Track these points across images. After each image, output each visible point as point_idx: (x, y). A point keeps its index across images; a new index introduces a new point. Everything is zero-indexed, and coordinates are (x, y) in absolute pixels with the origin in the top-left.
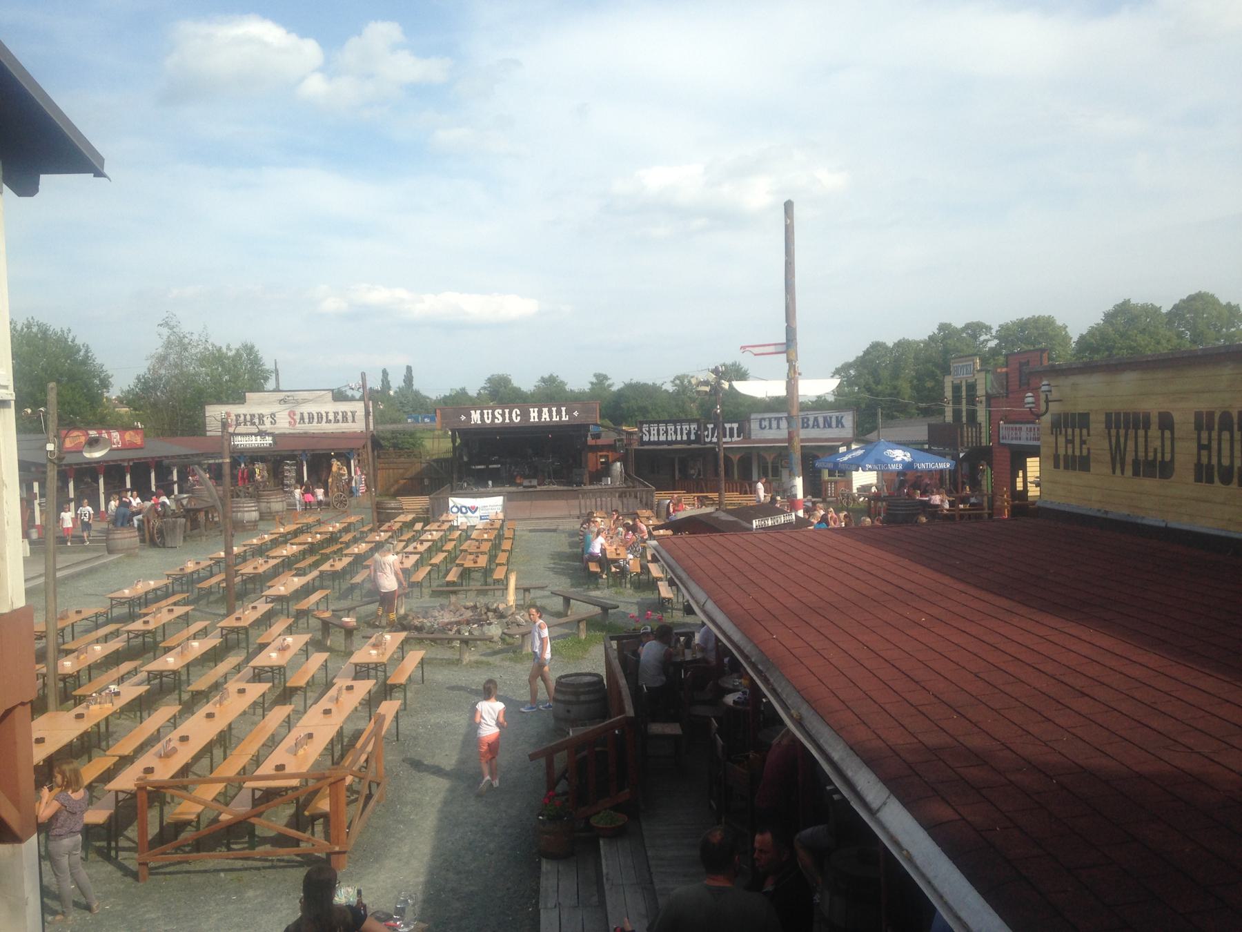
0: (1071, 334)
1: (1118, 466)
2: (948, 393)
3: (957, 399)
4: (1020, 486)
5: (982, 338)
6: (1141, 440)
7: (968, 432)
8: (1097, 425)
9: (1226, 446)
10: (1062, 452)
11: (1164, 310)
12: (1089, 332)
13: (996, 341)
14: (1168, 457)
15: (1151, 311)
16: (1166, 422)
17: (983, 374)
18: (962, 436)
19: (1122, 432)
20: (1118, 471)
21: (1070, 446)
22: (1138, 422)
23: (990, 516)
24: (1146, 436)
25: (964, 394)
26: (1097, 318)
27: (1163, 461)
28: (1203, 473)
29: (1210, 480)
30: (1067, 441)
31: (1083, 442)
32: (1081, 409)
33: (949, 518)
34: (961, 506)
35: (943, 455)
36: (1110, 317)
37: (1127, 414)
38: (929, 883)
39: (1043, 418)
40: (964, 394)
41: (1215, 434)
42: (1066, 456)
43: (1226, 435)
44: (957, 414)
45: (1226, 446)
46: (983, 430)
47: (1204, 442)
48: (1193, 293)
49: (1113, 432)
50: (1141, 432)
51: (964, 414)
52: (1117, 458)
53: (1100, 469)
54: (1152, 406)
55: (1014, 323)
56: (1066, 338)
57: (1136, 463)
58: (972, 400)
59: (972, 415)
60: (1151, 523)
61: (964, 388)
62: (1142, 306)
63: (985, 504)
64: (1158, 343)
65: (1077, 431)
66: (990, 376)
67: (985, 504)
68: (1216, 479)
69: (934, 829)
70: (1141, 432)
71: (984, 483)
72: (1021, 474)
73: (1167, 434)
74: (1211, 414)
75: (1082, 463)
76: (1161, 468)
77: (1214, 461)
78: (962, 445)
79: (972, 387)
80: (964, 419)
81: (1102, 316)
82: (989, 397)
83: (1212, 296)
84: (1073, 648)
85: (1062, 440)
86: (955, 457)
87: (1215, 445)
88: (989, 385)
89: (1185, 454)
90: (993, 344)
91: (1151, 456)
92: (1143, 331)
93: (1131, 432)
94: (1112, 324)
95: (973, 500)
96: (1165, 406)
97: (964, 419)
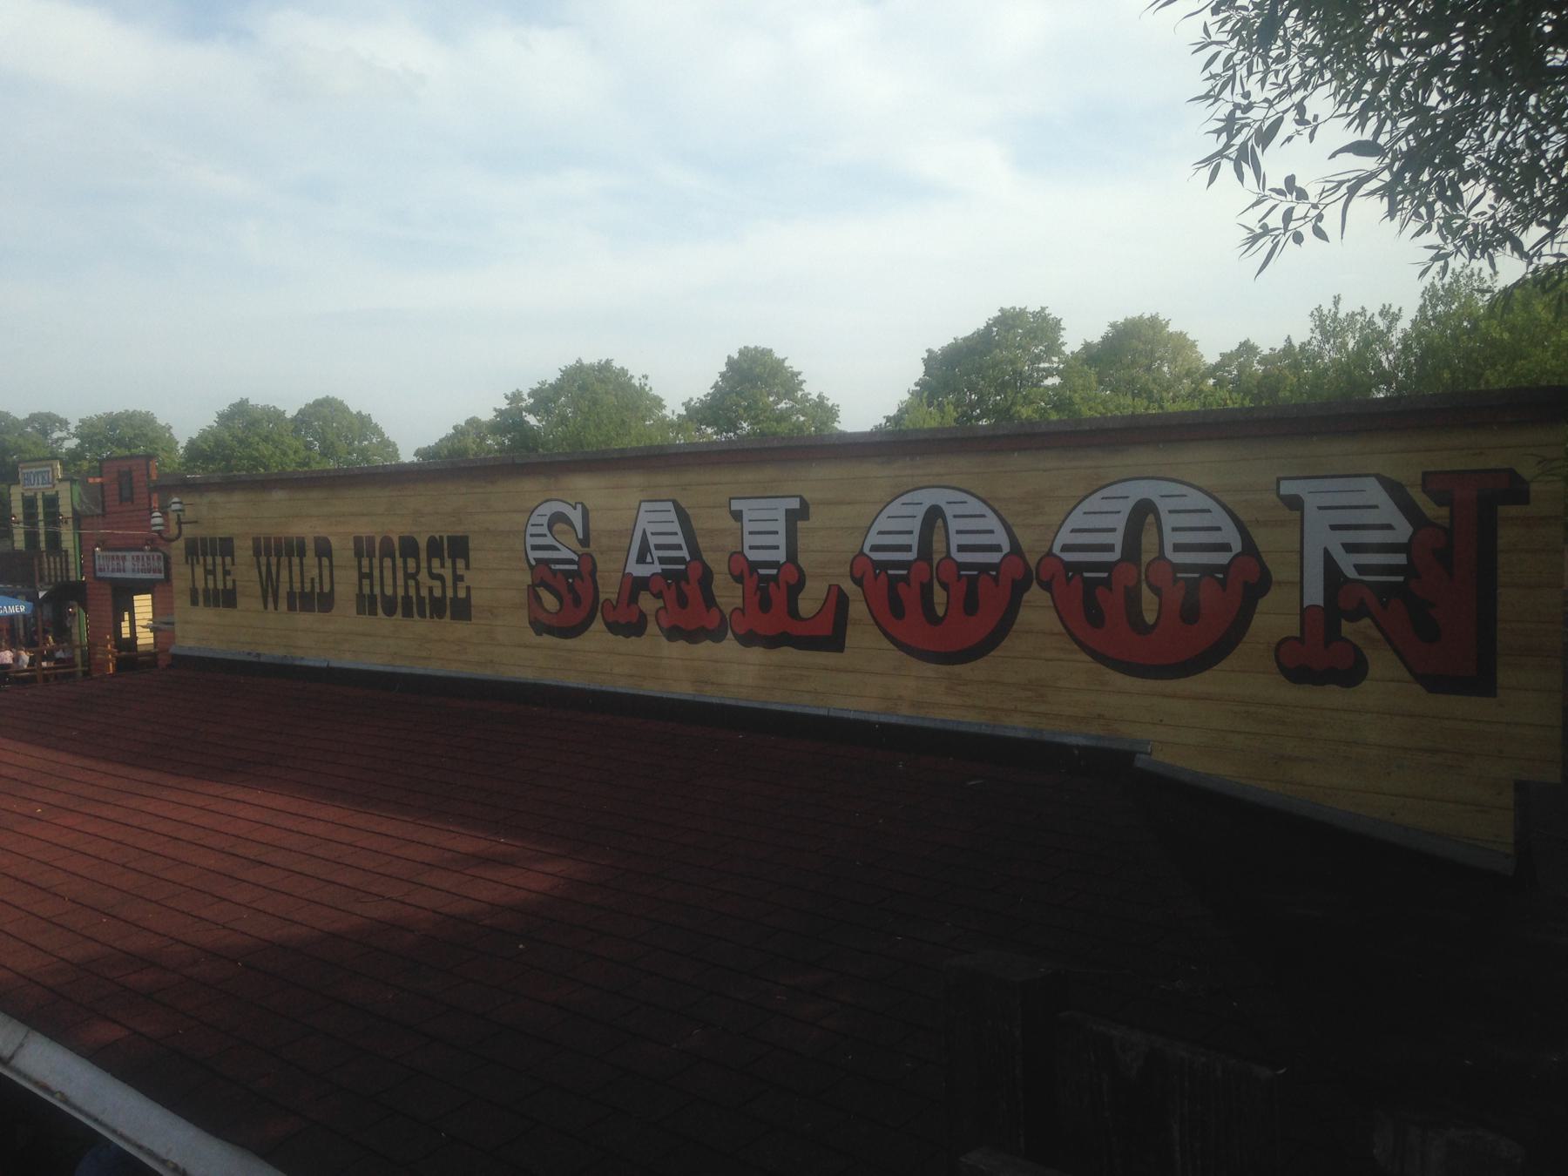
0: (177, 438)
1: (270, 599)
2: (17, 509)
3: (30, 516)
4: (126, 632)
5: (56, 435)
6: (296, 570)
7: (49, 564)
8: (243, 551)
9: (388, 574)
10: (200, 585)
11: (288, 415)
12: (200, 436)
13: (76, 441)
14: (326, 589)
15: (275, 416)
16: (324, 549)
17: (67, 484)
18: (41, 570)
19: (274, 560)
20: (271, 606)
21: (210, 577)
22: (295, 548)
23: (85, 674)
24: (301, 564)
25: (40, 510)
26: (209, 420)
27: (321, 593)
28: (366, 604)
29: (373, 612)
30: (207, 572)
31: (226, 573)
32: (222, 533)
33: (30, 680)
34: (44, 664)
35: (14, 595)
36: (225, 418)
37: (278, 540)
38: (96, 1120)
39: (174, 544)
40: (40, 510)
41: (376, 562)
42: (206, 590)
43: (388, 562)
44: (31, 537)
45: (388, 574)
46: (71, 559)
47: (366, 570)
48: (320, 397)
49: (263, 560)
50: (296, 560)
51: (42, 538)
52: (269, 591)
53: (249, 602)
54: (307, 529)
55: (100, 418)
56: (172, 442)
57: (291, 595)
58: (53, 516)
59: (54, 540)
60: (311, 663)
61: (40, 503)
62: (263, 408)
63: (78, 659)
64: (285, 454)
65: (219, 560)
66: (77, 488)
67: (78, 659)
68: (380, 610)
69: (102, 1057)
70: (296, 560)
71: (75, 631)
72: (127, 617)
73: (325, 561)
74: (371, 540)
75: (227, 598)
76: (318, 600)
77: (377, 590)
78: (42, 579)
79: (52, 502)
80: (43, 545)
81: (215, 417)
82: (78, 518)
83: (341, 403)
84: (241, 814)
85: (199, 571)
86: (31, 598)
87: (376, 573)
88: (76, 499)
89: (346, 585)
90: (72, 443)
91: (308, 588)
92: (266, 439)
93: (284, 560)
94: (228, 427)
95: (59, 654)
96: (322, 530)
97: (43, 545)
